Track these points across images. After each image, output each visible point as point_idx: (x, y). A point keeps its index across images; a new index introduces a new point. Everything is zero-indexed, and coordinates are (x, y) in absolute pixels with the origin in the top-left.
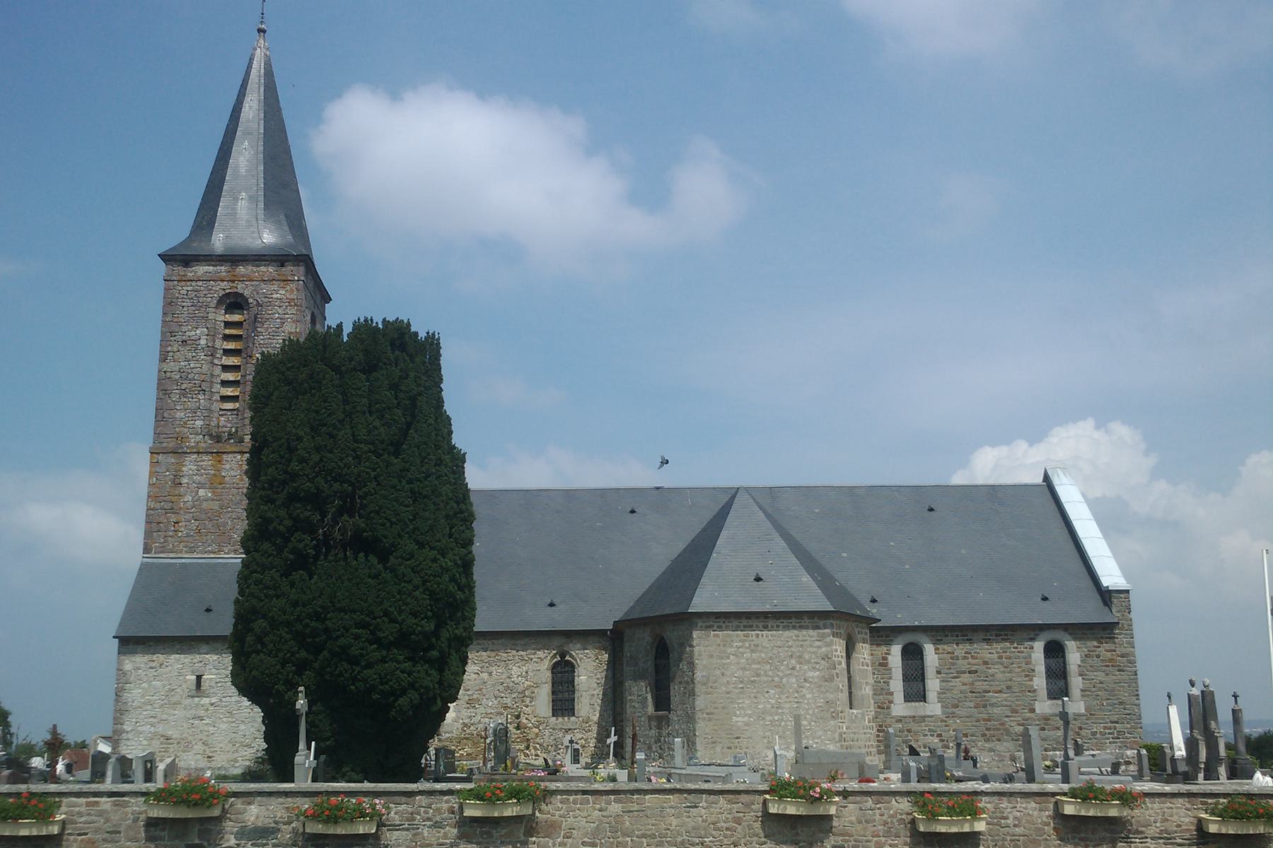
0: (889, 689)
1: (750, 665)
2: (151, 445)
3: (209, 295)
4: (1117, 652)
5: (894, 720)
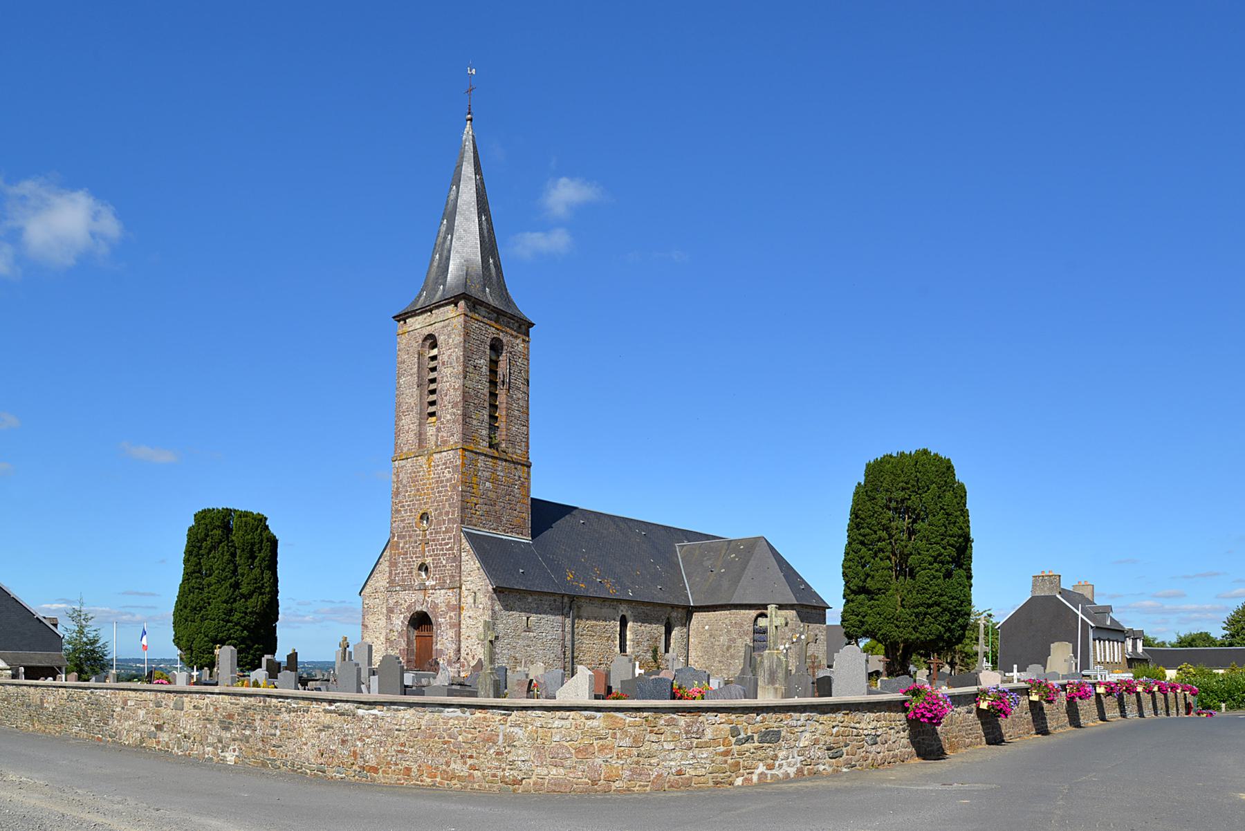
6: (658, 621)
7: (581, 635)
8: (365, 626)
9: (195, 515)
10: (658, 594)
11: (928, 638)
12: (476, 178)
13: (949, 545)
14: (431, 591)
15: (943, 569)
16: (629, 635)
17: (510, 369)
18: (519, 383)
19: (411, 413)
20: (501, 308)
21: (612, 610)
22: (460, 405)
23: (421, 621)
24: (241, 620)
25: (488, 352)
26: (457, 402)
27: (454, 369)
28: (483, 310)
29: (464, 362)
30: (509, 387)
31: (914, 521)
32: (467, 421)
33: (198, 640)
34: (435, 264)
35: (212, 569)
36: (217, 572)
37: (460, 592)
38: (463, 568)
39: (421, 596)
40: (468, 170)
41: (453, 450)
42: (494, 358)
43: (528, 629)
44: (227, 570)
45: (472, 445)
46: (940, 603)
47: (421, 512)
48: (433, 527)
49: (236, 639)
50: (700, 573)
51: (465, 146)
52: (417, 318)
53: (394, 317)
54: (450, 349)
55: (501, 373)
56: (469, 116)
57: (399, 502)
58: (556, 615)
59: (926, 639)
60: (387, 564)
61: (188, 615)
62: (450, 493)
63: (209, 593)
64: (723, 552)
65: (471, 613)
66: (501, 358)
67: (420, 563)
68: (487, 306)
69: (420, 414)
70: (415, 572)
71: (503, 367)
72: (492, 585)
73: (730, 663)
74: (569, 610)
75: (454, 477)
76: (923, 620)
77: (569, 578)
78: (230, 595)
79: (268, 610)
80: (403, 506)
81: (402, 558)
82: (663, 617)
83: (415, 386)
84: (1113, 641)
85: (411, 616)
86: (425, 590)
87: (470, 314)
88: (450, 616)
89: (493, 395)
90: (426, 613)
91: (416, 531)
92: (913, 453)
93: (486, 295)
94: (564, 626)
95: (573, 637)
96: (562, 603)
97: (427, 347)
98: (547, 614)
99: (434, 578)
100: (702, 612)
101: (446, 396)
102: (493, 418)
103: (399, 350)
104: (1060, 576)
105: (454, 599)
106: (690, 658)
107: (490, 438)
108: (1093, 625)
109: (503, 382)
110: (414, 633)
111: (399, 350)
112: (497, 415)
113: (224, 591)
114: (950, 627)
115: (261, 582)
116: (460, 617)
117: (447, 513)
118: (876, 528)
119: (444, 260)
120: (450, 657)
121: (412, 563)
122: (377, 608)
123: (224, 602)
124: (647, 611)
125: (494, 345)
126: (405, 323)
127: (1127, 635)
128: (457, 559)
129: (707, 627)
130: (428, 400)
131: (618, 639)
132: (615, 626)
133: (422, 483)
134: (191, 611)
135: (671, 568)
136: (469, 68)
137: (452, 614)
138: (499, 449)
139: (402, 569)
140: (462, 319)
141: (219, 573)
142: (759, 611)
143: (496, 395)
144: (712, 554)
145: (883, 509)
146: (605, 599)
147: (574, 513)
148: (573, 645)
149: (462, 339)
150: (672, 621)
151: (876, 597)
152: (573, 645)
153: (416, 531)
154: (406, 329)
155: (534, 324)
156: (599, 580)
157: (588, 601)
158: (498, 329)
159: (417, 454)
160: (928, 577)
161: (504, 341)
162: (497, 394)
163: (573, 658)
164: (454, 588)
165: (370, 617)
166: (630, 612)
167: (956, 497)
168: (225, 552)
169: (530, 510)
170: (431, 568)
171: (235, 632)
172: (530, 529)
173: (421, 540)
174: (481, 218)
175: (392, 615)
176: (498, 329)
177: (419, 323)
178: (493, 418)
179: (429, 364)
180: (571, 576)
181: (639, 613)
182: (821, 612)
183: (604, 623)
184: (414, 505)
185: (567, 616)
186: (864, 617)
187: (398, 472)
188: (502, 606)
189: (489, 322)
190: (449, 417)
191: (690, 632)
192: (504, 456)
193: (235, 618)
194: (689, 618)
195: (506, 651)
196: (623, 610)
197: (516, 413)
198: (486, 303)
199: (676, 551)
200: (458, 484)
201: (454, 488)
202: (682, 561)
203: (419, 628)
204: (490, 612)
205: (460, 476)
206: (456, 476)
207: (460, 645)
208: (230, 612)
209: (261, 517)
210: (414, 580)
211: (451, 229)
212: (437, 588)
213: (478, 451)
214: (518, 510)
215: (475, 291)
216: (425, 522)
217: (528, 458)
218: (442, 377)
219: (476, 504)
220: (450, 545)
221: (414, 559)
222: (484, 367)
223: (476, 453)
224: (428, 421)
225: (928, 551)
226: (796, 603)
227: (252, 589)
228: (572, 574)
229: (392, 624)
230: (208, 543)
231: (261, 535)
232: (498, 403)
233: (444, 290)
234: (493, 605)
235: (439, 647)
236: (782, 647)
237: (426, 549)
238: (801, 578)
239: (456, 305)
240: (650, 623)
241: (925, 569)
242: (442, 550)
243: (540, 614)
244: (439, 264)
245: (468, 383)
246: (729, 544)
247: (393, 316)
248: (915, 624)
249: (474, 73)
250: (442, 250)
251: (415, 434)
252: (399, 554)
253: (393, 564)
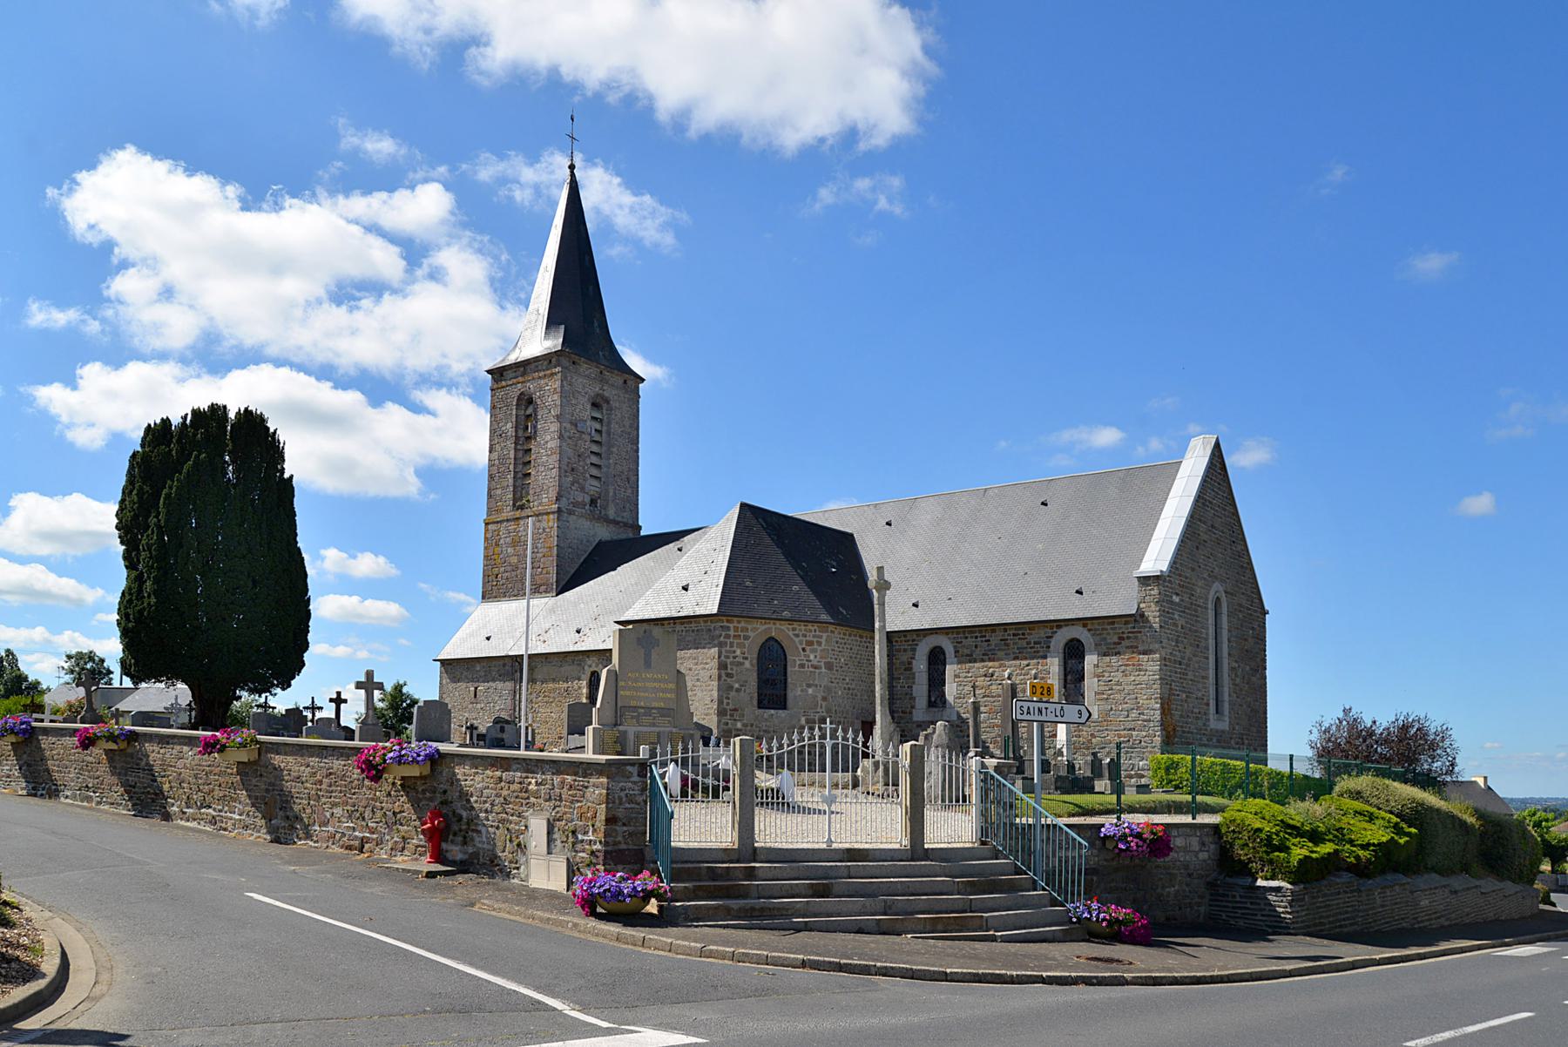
0: (912, 694)
2: (485, 517)
4: (1139, 648)
5: (915, 725)
92: (206, 410)
157: (543, 660)
183: (565, 685)
188: (449, 679)
223: (498, 522)
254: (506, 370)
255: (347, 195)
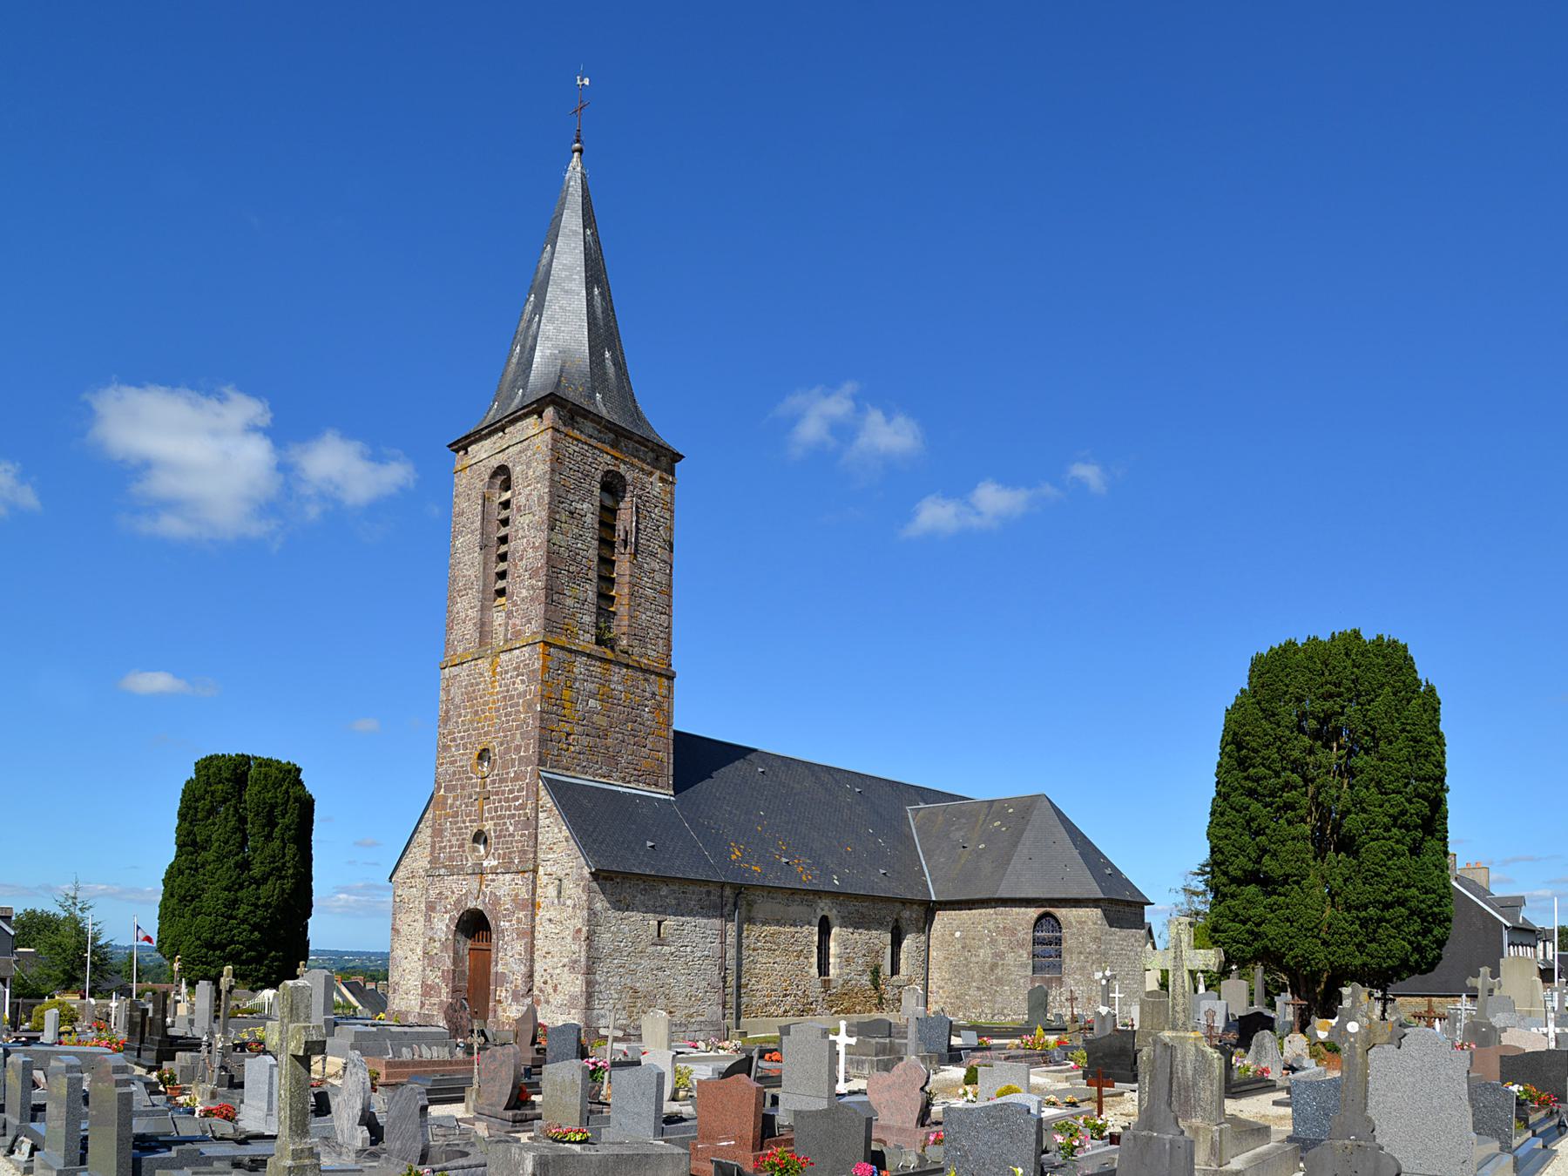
1: (159, 1068)
3: (594, 465)
6: (878, 924)
7: (754, 950)
8: (395, 930)
9: (196, 764)
10: (880, 882)
11: (1384, 965)
12: (584, 232)
13: (1418, 795)
14: (490, 877)
15: (1408, 839)
16: (834, 948)
17: (637, 522)
18: (655, 546)
19: (470, 592)
20: (623, 425)
21: (806, 907)
22: (542, 572)
23: (474, 925)
24: (250, 916)
25: (597, 491)
26: (538, 568)
27: (534, 516)
28: (589, 427)
29: (550, 503)
30: (636, 550)
31: (1351, 753)
32: (555, 598)
33: (186, 944)
34: (514, 360)
35: (210, 840)
36: (217, 844)
37: (535, 878)
38: (540, 838)
39: (476, 885)
40: (572, 220)
41: (529, 645)
42: (609, 503)
43: (660, 940)
44: (231, 842)
45: (564, 638)
46: (1406, 900)
47: (480, 748)
48: (496, 772)
49: (242, 943)
50: (946, 849)
51: (568, 187)
52: (483, 443)
53: (449, 446)
54: (529, 485)
55: (622, 528)
56: (577, 145)
57: (449, 734)
58: (709, 917)
59: (1380, 966)
60: (429, 831)
61: (176, 907)
62: (522, 716)
63: (204, 875)
64: (982, 818)
65: (552, 914)
66: (622, 505)
67: (475, 830)
68: (597, 419)
69: (483, 592)
70: (468, 844)
71: (625, 519)
72: (590, 867)
73: (996, 991)
74: (733, 908)
75: (530, 690)
76: (1375, 931)
77: (734, 857)
78: (233, 879)
79: (292, 902)
80: (454, 740)
81: (450, 822)
82: (889, 919)
83: (477, 549)
84: (1526, 946)
85: (460, 917)
86: (482, 874)
87: (563, 429)
88: (518, 918)
89: (607, 562)
90: (481, 911)
91: (471, 778)
93: (594, 403)
94: (724, 934)
95: (739, 951)
96: (722, 897)
97: (498, 486)
98: (694, 916)
99: (496, 855)
100: (949, 910)
101: (522, 560)
102: (605, 598)
103: (456, 496)
104: (1455, 855)
105: (524, 889)
106: (930, 981)
107: (598, 627)
108: (1508, 924)
109: (625, 542)
110: (466, 945)
111: (456, 496)
112: (613, 593)
113: (225, 874)
114: (1419, 944)
115: (282, 861)
116: (533, 919)
117: (518, 749)
118: (1277, 766)
119: (526, 352)
120: (516, 986)
121: (464, 831)
122: (414, 902)
123: (225, 889)
124: (864, 910)
125: (611, 483)
126: (466, 453)
127: (1538, 937)
128: (532, 824)
129: (958, 934)
130: (496, 571)
131: (815, 955)
132: (811, 934)
133: (481, 701)
134: (180, 901)
135: (901, 843)
136: (578, 77)
137: (521, 915)
138: (617, 649)
139: (450, 841)
140: (548, 436)
141: (220, 846)
142: (1042, 910)
143: (613, 563)
144: (964, 821)
145: (1292, 732)
146: (794, 891)
147: (748, 757)
148: (739, 965)
149: (547, 468)
150: (903, 924)
151: (1281, 890)
152: (739, 965)
153: (471, 778)
154: (468, 461)
155: (683, 457)
156: (784, 860)
157: (765, 894)
158: (617, 459)
159: (476, 656)
160: (1384, 853)
161: (629, 477)
162: (614, 562)
163: (739, 987)
164: (525, 872)
165: (403, 917)
166: (834, 911)
167: (1425, 711)
168: (230, 816)
169: (671, 747)
170: (492, 840)
171: (240, 933)
172: (672, 778)
173: (479, 793)
174: (593, 292)
175: (433, 915)
176: (617, 459)
177: (486, 451)
178: (605, 598)
179: (499, 513)
180: (738, 853)
181: (849, 914)
182: (1138, 910)
183: (792, 929)
184: (469, 736)
185: (728, 918)
186: (1258, 925)
187: (448, 686)
188: (609, 902)
189: (599, 445)
190: (524, 593)
191: (931, 941)
192: (624, 659)
193: (240, 913)
194: (929, 920)
195: (616, 979)
196: (825, 908)
197: (649, 592)
198: (595, 414)
199: (908, 818)
200: (536, 699)
201: (529, 706)
202: (917, 832)
203: (474, 937)
204: (585, 913)
205: (538, 687)
206: (533, 687)
207: (532, 967)
208: (233, 905)
209: (290, 767)
210: (467, 858)
211: (539, 308)
212: (499, 871)
213: (575, 648)
214: (649, 746)
215: (573, 395)
216: (486, 764)
217: (670, 665)
218: (517, 531)
219: (569, 734)
220: (521, 801)
221: (468, 824)
222: (589, 515)
223: (570, 651)
224: (496, 604)
225: (1381, 806)
226: (1103, 896)
227: (267, 869)
228: (739, 850)
229: (432, 928)
230: (207, 802)
231: (287, 792)
232: (615, 575)
233: (524, 395)
234: (590, 901)
235: (500, 968)
236: (1098, 975)
237: (486, 808)
238: (1105, 858)
239: (540, 416)
240: (868, 929)
241: (1377, 839)
242: (509, 808)
243: (682, 915)
244: (519, 359)
245: (557, 538)
246: (991, 807)
247: (448, 444)
248: (1360, 938)
249: (587, 83)
250: (526, 339)
251: (475, 624)
252: (447, 817)
253: (438, 833)
254: (585, 417)
255: (1314, 642)
